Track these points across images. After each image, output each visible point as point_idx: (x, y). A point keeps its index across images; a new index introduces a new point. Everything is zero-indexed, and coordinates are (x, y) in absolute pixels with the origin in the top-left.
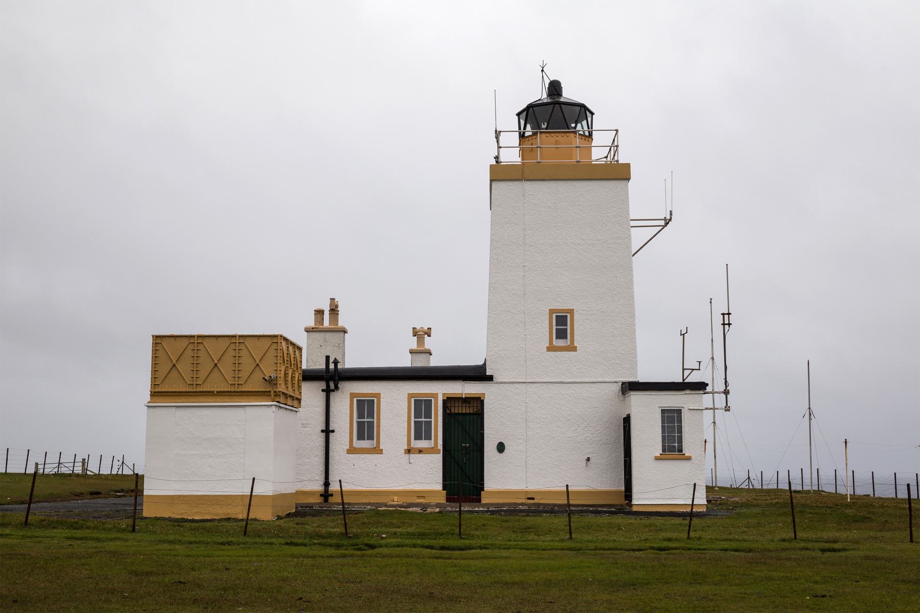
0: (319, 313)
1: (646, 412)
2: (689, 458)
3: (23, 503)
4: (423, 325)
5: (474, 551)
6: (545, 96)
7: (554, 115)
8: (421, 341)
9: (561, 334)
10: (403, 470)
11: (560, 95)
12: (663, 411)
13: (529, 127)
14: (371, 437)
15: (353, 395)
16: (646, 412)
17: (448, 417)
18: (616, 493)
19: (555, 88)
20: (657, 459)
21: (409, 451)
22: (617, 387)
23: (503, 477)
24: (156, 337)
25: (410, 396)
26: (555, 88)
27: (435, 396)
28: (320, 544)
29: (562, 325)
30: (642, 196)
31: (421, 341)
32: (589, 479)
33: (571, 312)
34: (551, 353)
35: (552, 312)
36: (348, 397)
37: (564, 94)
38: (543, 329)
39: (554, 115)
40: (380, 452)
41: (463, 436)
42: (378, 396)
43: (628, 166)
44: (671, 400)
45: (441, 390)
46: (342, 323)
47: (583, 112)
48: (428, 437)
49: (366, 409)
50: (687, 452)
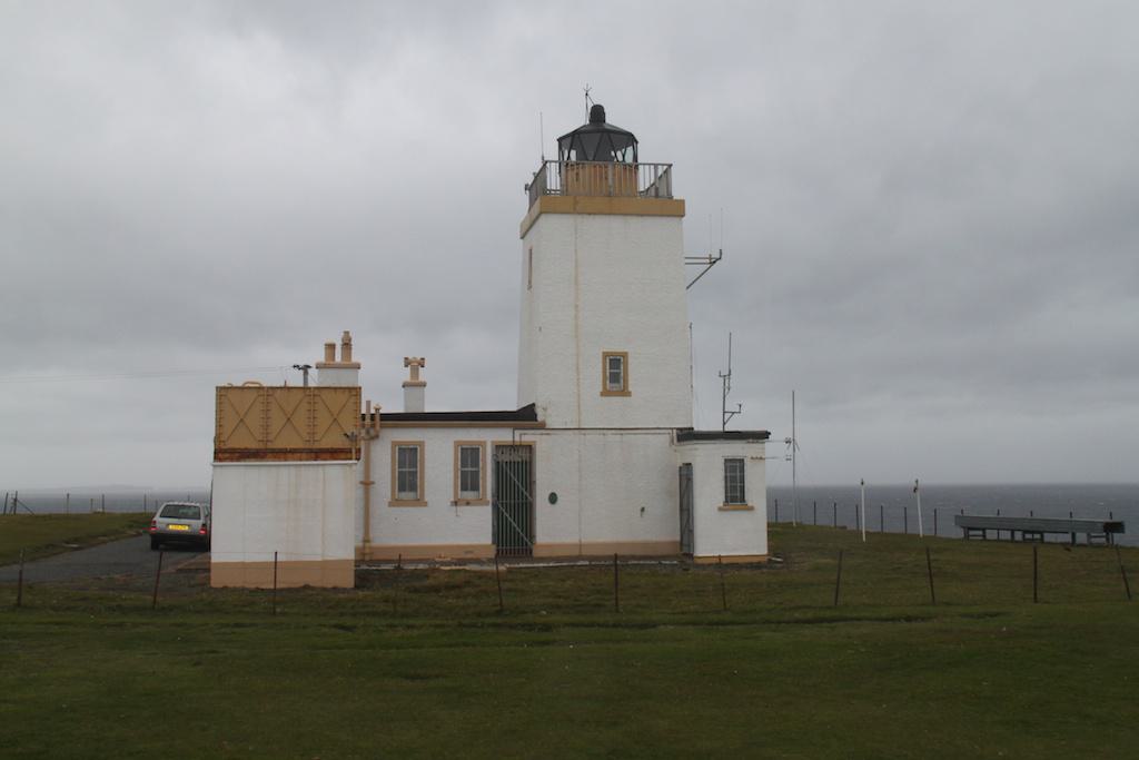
0: (331, 347)
2: (752, 509)
4: (415, 354)
7: (597, 144)
8: (415, 373)
9: (615, 378)
13: (573, 153)
14: (413, 488)
15: (394, 444)
16: (708, 464)
17: (499, 468)
18: (674, 543)
19: (597, 113)
21: (456, 503)
23: (554, 529)
24: (219, 389)
25: (457, 444)
26: (597, 113)
27: (483, 444)
29: (615, 368)
30: (695, 232)
31: (415, 373)
32: (649, 529)
33: (625, 355)
34: (605, 399)
35: (606, 355)
36: (390, 446)
37: (607, 121)
38: (595, 373)
39: (597, 144)
40: (425, 504)
42: (422, 444)
43: (683, 202)
45: (489, 437)
46: (355, 359)
47: (629, 139)
48: (475, 487)
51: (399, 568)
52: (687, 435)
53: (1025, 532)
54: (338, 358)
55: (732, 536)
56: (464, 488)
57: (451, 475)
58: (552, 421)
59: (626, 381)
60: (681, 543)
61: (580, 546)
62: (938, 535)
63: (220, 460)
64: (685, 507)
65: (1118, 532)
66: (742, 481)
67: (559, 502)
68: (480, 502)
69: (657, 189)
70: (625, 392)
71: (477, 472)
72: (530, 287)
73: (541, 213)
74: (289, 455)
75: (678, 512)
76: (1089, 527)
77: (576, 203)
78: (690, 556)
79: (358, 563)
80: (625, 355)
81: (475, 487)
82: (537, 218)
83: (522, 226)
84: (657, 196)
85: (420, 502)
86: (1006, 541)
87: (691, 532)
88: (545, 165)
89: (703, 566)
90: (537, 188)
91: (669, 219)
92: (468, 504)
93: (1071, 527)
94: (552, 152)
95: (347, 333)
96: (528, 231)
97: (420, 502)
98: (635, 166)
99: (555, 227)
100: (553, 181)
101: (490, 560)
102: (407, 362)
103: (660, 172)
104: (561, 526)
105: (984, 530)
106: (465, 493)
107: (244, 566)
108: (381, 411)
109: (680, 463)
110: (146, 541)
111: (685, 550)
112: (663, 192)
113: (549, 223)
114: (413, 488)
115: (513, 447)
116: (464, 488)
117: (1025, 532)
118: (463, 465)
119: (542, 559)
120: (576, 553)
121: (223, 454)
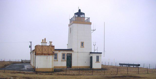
0: (43, 40)
1: (94, 57)
3: (34, 69)
4: (51, 41)
6: (78, 11)
7: (79, 14)
8: (51, 44)
9: (82, 45)
14: (56, 59)
18: (89, 66)
19: (80, 10)
21: (62, 61)
23: (74, 64)
26: (80, 10)
29: (82, 44)
33: (84, 42)
35: (81, 42)
38: (80, 44)
39: (79, 14)
41: (69, 59)
42: (57, 53)
44: (98, 55)
45: (66, 52)
47: (84, 14)
50: (99, 61)
52: (91, 53)
54: (44, 41)
56: (55, 59)
58: (74, 51)
68: (65, 61)
70: (83, 47)
71: (57, 57)
72: (71, 33)
80: (84, 42)
90: (71, 20)
99: (75, 25)
102: (50, 42)
114: (56, 59)
115: (69, 54)
116: (55, 59)
118: (63, 56)
119: (73, 68)
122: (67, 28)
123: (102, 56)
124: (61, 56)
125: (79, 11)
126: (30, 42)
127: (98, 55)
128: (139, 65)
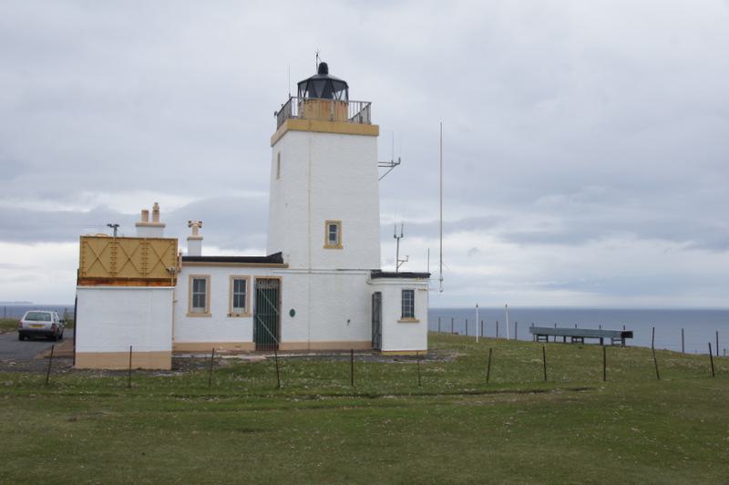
2: (418, 321)
4: (334, 218)
5: (502, 390)
7: (322, 86)
9: (333, 237)
10: (230, 330)
11: (327, 73)
12: (403, 291)
15: (191, 276)
17: (258, 293)
18: (367, 343)
19: (323, 68)
20: (399, 322)
22: (369, 273)
23: (293, 333)
25: (232, 277)
26: (323, 68)
28: (504, 392)
29: (333, 230)
30: (384, 147)
31: (195, 231)
33: (339, 223)
34: (327, 251)
35: (327, 222)
36: (187, 277)
38: (321, 233)
39: (322, 86)
40: (210, 316)
41: (267, 306)
42: (209, 277)
45: (252, 274)
46: (162, 220)
47: (344, 85)
49: (199, 285)
51: (193, 357)
52: (377, 274)
53: (573, 337)
55: (403, 338)
56: (236, 305)
57: (228, 297)
59: (340, 239)
60: (373, 343)
61: (309, 344)
62: (518, 339)
63: (83, 285)
64: (376, 318)
65: (434, 333)
66: (413, 303)
67: (296, 315)
68: (246, 314)
69: (361, 118)
70: (339, 247)
71: (244, 296)
73: (288, 130)
74: (129, 283)
75: (371, 323)
76: (612, 334)
77: (310, 124)
78: (380, 351)
79: (174, 352)
80: (339, 223)
81: (242, 305)
82: (285, 133)
83: (272, 138)
84: (361, 122)
85: (207, 314)
86: (560, 343)
87: (380, 335)
88: (290, 100)
89: (388, 357)
90: (283, 115)
91: (362, 138)
92: (238, 316)
93: (601, 335)
94: (295, 92)
95: (156, 204)
96: (276, 142)
97: (207, 314)
98: (346, 103)
99: (295, 140)
100: (295, 111)
101: (252, 352)
103: (364, 106)
104: (302, 328)
105: (547, 336)
106: (236, 309)
107: (97, 355)
108: (183, 255)
109: (372, 292)
110: (17, 335)
111: (375, 347)
112: (365, 120)
113: (292, 138)
114: (202, 305)
115: (269, 280)
116: (236, 305)
117: (573, 337)
120: (306, 348)
121: (83, 280)
122: (268, 154)
123: (431, 293)
124: (187, 293)
125: (319, 73)
126: (111, 226)
127: (411, 287)
128: (628, 335)
